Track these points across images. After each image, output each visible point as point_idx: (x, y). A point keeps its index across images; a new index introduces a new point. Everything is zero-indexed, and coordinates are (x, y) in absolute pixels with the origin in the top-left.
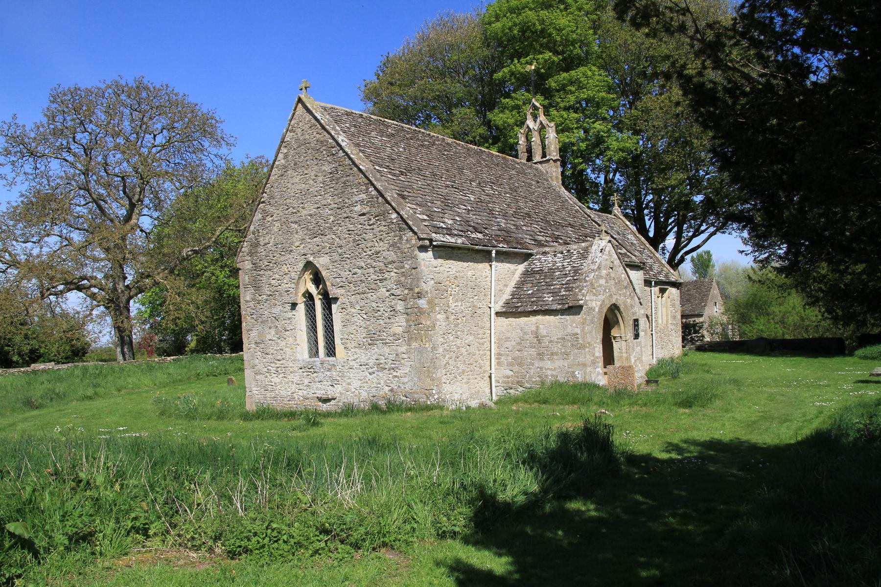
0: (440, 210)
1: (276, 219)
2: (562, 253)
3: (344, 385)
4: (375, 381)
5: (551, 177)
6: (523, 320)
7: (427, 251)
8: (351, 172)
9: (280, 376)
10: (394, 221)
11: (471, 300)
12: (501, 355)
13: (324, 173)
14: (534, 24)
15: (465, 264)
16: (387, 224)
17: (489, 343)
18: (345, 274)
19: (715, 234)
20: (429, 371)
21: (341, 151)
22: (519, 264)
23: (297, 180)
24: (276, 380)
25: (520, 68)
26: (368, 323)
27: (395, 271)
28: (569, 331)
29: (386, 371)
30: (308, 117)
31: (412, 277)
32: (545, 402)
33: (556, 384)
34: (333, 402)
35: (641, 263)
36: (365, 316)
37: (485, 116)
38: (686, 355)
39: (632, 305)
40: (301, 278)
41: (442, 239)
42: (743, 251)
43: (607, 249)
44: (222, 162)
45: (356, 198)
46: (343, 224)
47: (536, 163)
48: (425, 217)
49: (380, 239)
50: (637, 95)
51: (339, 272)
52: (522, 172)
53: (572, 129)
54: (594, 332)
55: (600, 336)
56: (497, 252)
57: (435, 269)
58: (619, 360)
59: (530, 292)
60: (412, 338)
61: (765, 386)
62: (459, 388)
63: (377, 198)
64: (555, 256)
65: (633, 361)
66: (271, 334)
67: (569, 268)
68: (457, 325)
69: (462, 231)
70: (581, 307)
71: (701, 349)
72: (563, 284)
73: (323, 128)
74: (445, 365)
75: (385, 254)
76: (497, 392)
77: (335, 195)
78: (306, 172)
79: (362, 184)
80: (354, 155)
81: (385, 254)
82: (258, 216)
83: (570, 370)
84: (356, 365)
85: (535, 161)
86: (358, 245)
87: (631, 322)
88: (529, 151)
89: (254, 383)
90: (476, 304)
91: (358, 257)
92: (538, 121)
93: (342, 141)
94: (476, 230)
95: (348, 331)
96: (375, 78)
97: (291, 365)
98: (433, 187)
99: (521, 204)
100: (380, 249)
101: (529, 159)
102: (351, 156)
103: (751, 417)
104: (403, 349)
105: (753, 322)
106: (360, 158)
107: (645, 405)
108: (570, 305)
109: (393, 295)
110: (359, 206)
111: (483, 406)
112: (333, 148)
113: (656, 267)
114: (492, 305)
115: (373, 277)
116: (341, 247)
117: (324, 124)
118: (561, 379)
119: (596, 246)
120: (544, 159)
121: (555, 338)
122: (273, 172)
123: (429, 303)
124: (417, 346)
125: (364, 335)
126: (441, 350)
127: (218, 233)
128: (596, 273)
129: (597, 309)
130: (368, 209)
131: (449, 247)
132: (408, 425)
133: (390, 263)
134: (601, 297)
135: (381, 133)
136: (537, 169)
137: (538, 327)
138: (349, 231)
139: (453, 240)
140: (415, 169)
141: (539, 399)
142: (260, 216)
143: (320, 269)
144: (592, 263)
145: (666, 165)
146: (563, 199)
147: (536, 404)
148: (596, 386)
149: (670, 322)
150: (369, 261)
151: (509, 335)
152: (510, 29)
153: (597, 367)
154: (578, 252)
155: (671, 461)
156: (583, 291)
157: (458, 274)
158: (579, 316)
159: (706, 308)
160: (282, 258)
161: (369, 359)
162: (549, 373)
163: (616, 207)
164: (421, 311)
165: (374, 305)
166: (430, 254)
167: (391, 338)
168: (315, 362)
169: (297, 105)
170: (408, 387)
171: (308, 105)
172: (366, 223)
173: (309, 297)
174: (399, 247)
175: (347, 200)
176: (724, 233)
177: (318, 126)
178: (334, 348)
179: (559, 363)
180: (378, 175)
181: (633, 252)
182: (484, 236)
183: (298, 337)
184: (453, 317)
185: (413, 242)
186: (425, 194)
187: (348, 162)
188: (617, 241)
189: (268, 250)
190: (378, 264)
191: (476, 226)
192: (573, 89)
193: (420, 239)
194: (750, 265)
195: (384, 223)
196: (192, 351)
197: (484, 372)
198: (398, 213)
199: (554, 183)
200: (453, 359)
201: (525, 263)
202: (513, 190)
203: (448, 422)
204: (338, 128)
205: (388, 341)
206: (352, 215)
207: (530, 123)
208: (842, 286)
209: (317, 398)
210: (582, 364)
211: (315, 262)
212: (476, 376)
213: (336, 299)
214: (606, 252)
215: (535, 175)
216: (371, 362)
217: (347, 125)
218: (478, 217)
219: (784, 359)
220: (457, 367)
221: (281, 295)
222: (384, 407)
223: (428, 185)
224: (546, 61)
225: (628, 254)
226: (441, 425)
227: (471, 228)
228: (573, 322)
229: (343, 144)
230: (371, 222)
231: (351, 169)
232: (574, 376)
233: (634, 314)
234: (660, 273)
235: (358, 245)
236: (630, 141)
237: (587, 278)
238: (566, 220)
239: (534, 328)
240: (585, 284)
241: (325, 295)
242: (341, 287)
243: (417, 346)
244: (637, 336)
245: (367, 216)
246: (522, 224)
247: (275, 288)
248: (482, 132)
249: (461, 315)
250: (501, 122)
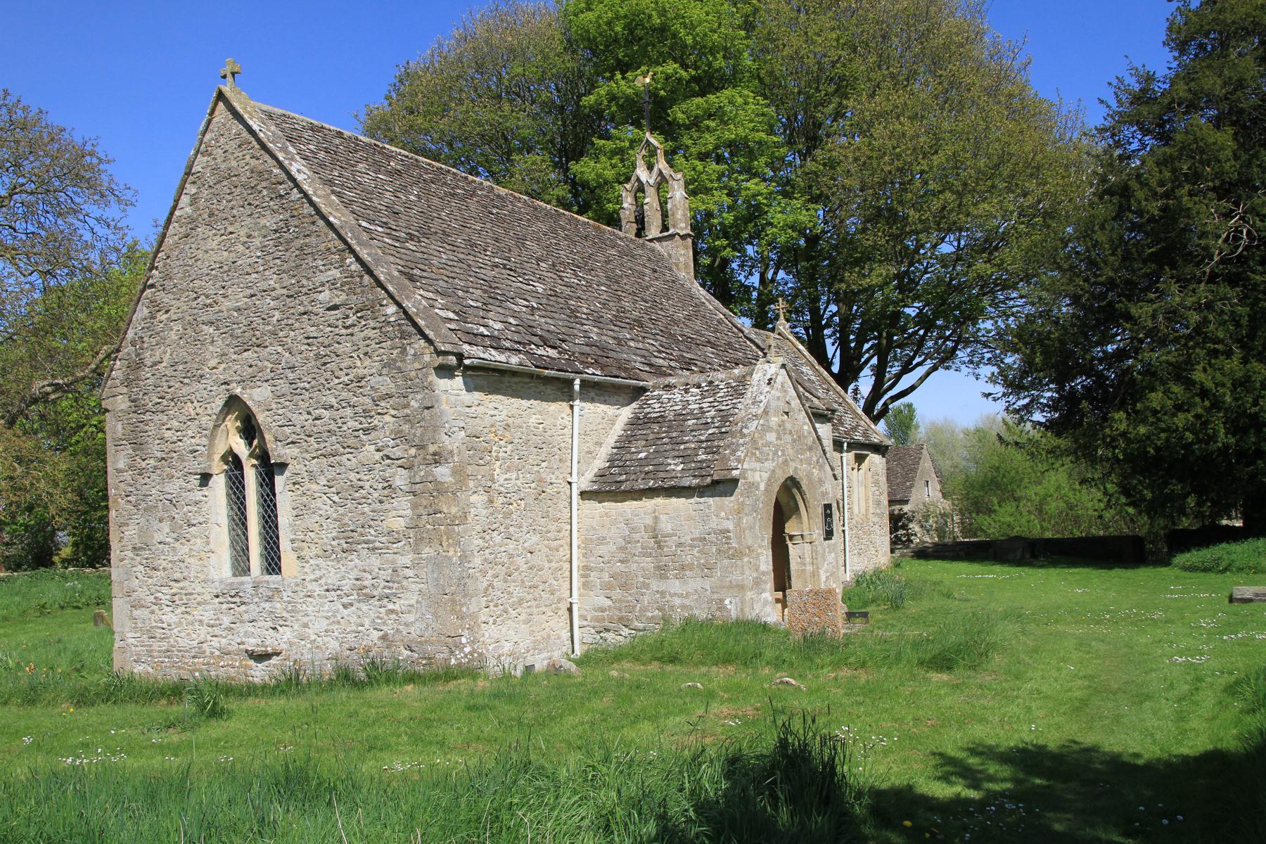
0: (479, 304)
1: (174, 317)
2: (699, 386)
3: (296, 627)
4: (354, 619)
5: (677, 265)
6: (630, 506)
7: (452, 376)
8: (314, 228)
9: (179, 611)
10: (392, 319)
11: (536, 468)
12: (590, 569)
13: (263, 232)
14: (650, 17)
15: (525, 403)
16: (378, 325)
17: (567, 548)
18: (299, 419)
19: (937, 369)
20: (453, 602)
21: (295, 190)
22: (623, 405)
23: (214, 245)
24: (170, 618)
25: (625, 88)
26: (341, 510)
27: (393, 412)
28: (714, 525)
29: (374, 602)
30: (236, 127)
31: (423, 424)
32: (673, 660)
33: (690, 624)
34: (274, 660)
35: (828, 409)
36: (336, 498)
37: (567, 169)
38: (898, 566)
39: (820, 480)
40: (219, 426)
41: (482, 355)
42: (990, 394)
43: (779, 379)
44: (109, 232)
45: (322, 278)
46: (297, 325)
47: (651, 241)
48: (452, 315)
49: (366, 354)
50: (814, 141)
51: (289, 415)
52: (626, 253)
53: (711, 189)
55: (768, 535)
56: (584, 384)
57: (467, 410)
58: (798, 577)
59: (642, 455)
60: (422, 539)
61: (1056, 622)
62: (511, 632)
63: (361, 277)
64: (687, 391)
65: (823, 578)
66: (163, 532)
67: (713, 413)
68: (508, 515)
69: (519, 343)
70: (735, 481)
71: (923, 554)
72: (702, 442)
73: (264, 147)
74: (487, 589)
75: (373, 380)
76: (584, 638)
77: (284, 272)
78: (230, 229)
79: (334, 250)
80: (319, 197)
81: (373, 380)
82: (143, 311)
83: (715, 596)
84: (317, 589)
85: (650, 237)
86: (325, 364)
87: (820, 510)
88: (640, 221)
89: (129, 623)
90: (544, 475)
91: (325, 387)
92: (655, 169)
93: (299, 171)
94: (546, 343)
95: (305, 525)
96: (386, 103)
97: (198, 589)
98: (469, 266)
99: (626, 304)
100: (366, 371)
101: (639, 233)
102: (315, 199)
103: (1070, 690)
104: (406, 560)
105: (995, 511)
106: (331, 204)
107: (863, 665)
108: (716, 477)
109: (388, 457)
110: (327, 292)
111: (554, 670)
112: (281, 184)
113: (848, 419)
114: (574, 479)
115: (352, 424)
116: (292, 368)
117: (265, 140)
118: (702, 614)
119: (760, 374)
120: (666, 234)
121: (687, 539)
122: (171, 230)
123: (455, 472)
124: (433, 554)
125: (335, 534)
126: (477, 561)
127: (101, 356)
128: (762, 422)
129: (762, 487)
130: (343, 297)
131: (495, 370)
132: (404, 714)
133: (383, 398)
134: (769, 465)
135: (378, 168)
136: (653, 250)
137: (656, 518)
138: (308, 338)
139: (502, 358)
140: (436, 233)
141: (659, 655)
142: (146, 311)
143: (254, 409)
144: (753, 403)
145: (862, 253)
146: (697, 301)
147: (656, 663)
148: (765, 627)
149: (871, 511)
150: (344, 395)
151: (603, 532)
152: (609, 23)
153: (764, 591)
154: (728, 385)
155: (957, 806)
156: (739, 453)
157: (510, 421)
158: (732, 498)
159: (914, 490)
160: (185, 390)
161: (343, 578)
162: (677, 601)
163: (782, 320)
164: (440, 489)
165: (353, 476)
166: (459, 381)
167: (383, 539)
168: (242, 583)
169: (216, 104)
170: (415, 631)
171: (236, 104)
172: (340, 322)
173: (234, 462)
174: (399, 368)
175: (304, 282)
176: (948, 368)
177: (255, 143)
178: (279, 558)
179: (695, 584)
180: (365, 236)
181: (814, 392)
182: (560, 353)
183: (211, 537)
184: (501, 499)
185: (427, 358)
186: (453, 275)
187: (306, 209)
189: (158, 376)
190: (361, 399)
191: (544, 334)
192: (712, 124)
193: (439, 353)
194: (999, 418)
195: (372, 323)
196: (67, 562)
197: (559, 600)
198: (399, 305)
199: (682, 274)
200: (501, 577)
201: (634, 405)
202: (613, 280)
203: (483, 707)
204: (291, 149)
205: (377, 544)
206: (315, 309)
207: (642, 173)
208: (1152, 451)
209: (247, 651)
210: (738, 586)
211: (245, 397)
212: (544, 609)
213: (283, 466)
214: (778, 385)
215: (649, 260)
216: (347, 584)
217: (312, 147)
218: (549, 321)
219: (1058, 570)
220: (509, 593)
221: (181, 459)
222: (362, 675)
223: (460, 261)
224: (668, 78)
226: (467, 714)
227: (535, 339)
228: (722, 508)
229: (299, 177)
230: (349, 322)
231: (313, 223)
232: (722, 607)
233: (824, 494)
234: (854, 429)
235: (325, 364)
236: (804, 212)
237: (745, 431)
238: (702, 335)
239: (649, 521)
240: (741, 441)
241: (263, 457)
242: (293, 443)
243: (433, 554)
244: (829, 535)
245: (342, 309)
246: (628, 336)
247: (171, 446)
248: (562, 193)
249: (516, 497)
250: (593, 176)
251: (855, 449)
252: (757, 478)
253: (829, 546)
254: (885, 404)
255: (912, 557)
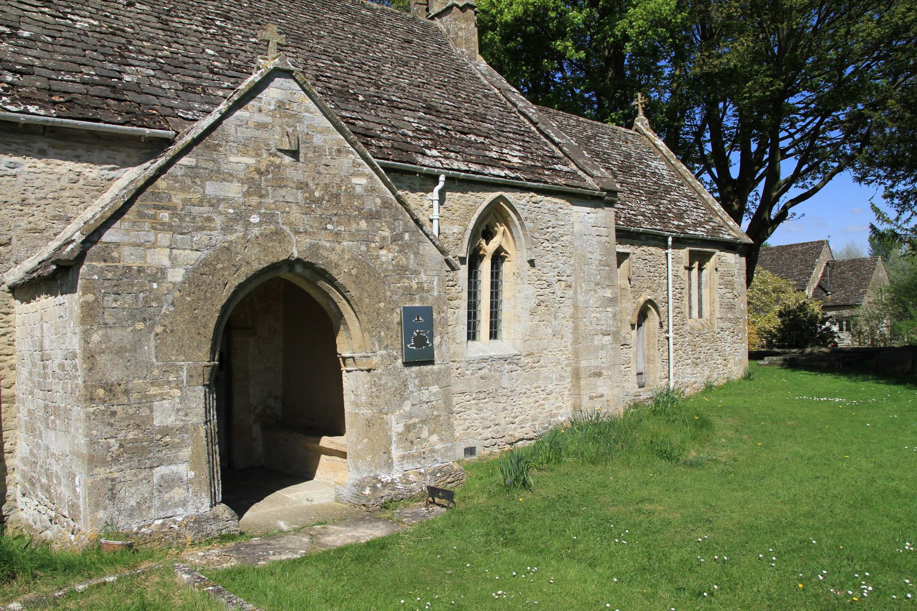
22: (125, 165)
35: (602, 190)
54: (149, 347)
85: (433, 14)
129: (177, 275)
134: (218, 237)
158: (76, 296)
181: (588, 169)
188: (561, 149)
225: (580, 173)
233: (409, 293)
251: (690, 245)
252: (159, 258)
253: (421, 376)
254: (785, 208)
255: (782, 365)
